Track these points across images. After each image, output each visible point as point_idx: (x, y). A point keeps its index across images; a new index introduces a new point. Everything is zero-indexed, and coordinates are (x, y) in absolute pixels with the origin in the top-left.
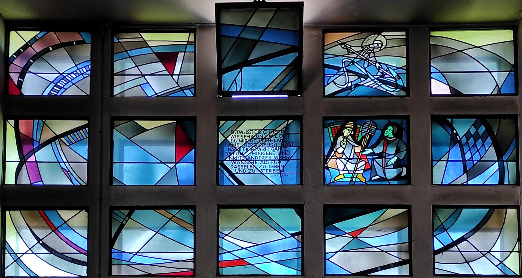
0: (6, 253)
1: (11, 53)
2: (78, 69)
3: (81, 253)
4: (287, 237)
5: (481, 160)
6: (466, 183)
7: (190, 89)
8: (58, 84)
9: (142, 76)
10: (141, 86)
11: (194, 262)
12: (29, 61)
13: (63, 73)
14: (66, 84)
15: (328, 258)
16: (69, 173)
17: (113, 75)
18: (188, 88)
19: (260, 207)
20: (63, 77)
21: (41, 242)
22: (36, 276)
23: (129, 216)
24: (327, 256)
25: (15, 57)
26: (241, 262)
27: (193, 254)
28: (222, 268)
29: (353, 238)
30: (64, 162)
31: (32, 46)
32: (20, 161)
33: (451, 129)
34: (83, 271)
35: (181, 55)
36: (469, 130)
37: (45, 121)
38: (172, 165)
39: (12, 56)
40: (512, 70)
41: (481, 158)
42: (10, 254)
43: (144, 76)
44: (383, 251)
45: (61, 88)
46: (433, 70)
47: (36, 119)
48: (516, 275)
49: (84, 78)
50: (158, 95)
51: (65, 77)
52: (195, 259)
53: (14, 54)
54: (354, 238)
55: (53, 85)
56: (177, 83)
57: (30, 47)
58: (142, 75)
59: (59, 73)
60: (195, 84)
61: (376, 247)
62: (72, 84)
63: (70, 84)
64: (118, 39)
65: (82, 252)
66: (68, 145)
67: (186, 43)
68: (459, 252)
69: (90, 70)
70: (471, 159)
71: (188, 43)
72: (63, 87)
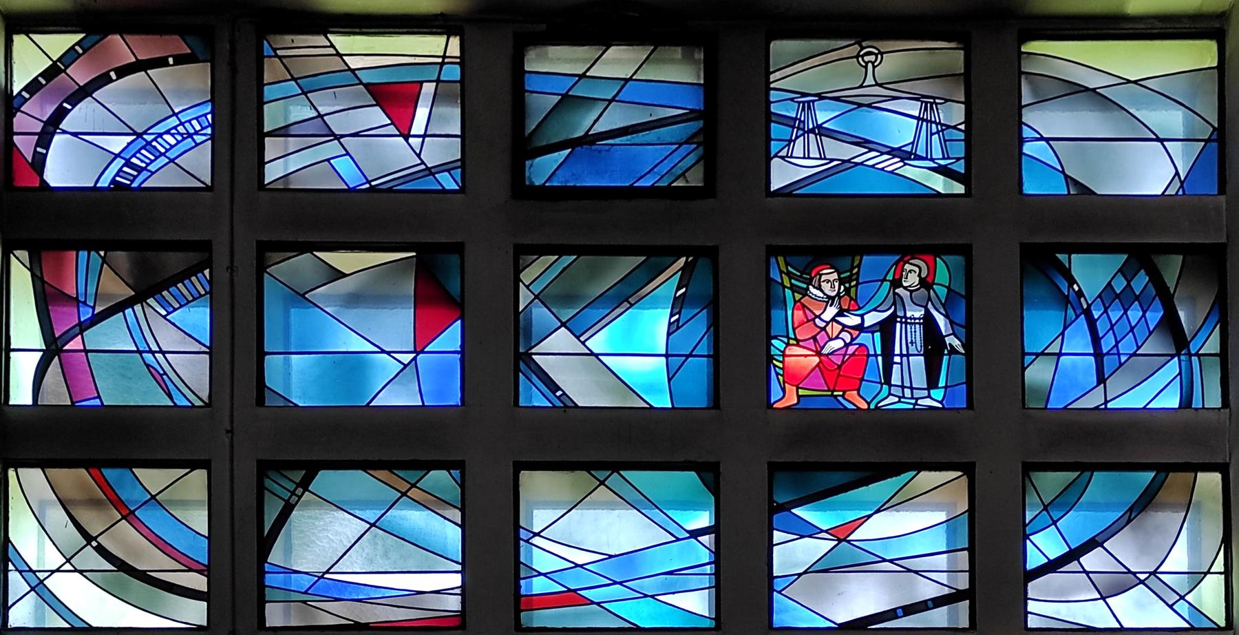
0: (11, 570)
1: (17, 89)
2: (182, 124)
3: (190, 570)
4: (680, 537)
5: (1138, 353)
6: (1103, 407)
7: (452, 172)
8: (134, 160)
9: (332, 138)
10: (332, 161)
11: (462, 64)
12: (61, 105)
13: (145, 132)
14: (152, 161)
15: (779, 589)
16: (165, 377)
17: (262, 135)
18: (446, 167)
19: (616, 467)
20: (144, 143)
21: (94, 544)
22: (87, 626)
23: (305, 484)
24: (778, 584)
25: (27, 96)
26: (571, 598)
27: (459, 140)
28: (528, 580)
29: (837, 542)
30: (153, 353)
31: (68, 71)
32: (44, 348)
33: (1067, 281)
34: (195, 613)
35: (428, 89)
36: (1109, 284)
37: (105, 254)
38: (406, 358)
39: (19, 93)
40: (1212, 138)
41: (1139, 348)
42: (20, 572)
43: (338, 137)
44: (909, 571)
45: (140, 170)
46: (1027, 132)
47: (83, 249)
48: (1219, 628)
49: (197, 145)
50: (373, 183)
51: (149, 143)
52: (465, 595)
53: (25, 89)
54: (840, 541)
55: (119, 162)
56: (419, 156)
57: (63, 74)
58: (333, 134)
59: (135, 133)
60: (463, 159)
61: (891, 561)
62: (168, 160)
63: (163, 160)
64: (275, 50)
65: (194, 568)
66: (164, 313)
67: (440, 60)
68: (1084, 575)
69: (210, 125)
70: (1115, 351)
71: (443, 60)
72: (145, 169)
